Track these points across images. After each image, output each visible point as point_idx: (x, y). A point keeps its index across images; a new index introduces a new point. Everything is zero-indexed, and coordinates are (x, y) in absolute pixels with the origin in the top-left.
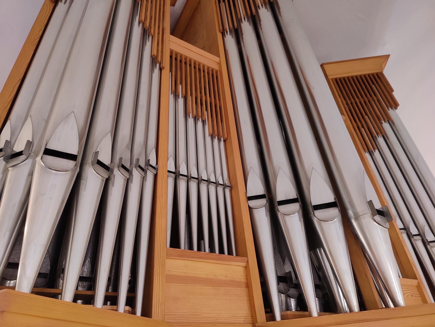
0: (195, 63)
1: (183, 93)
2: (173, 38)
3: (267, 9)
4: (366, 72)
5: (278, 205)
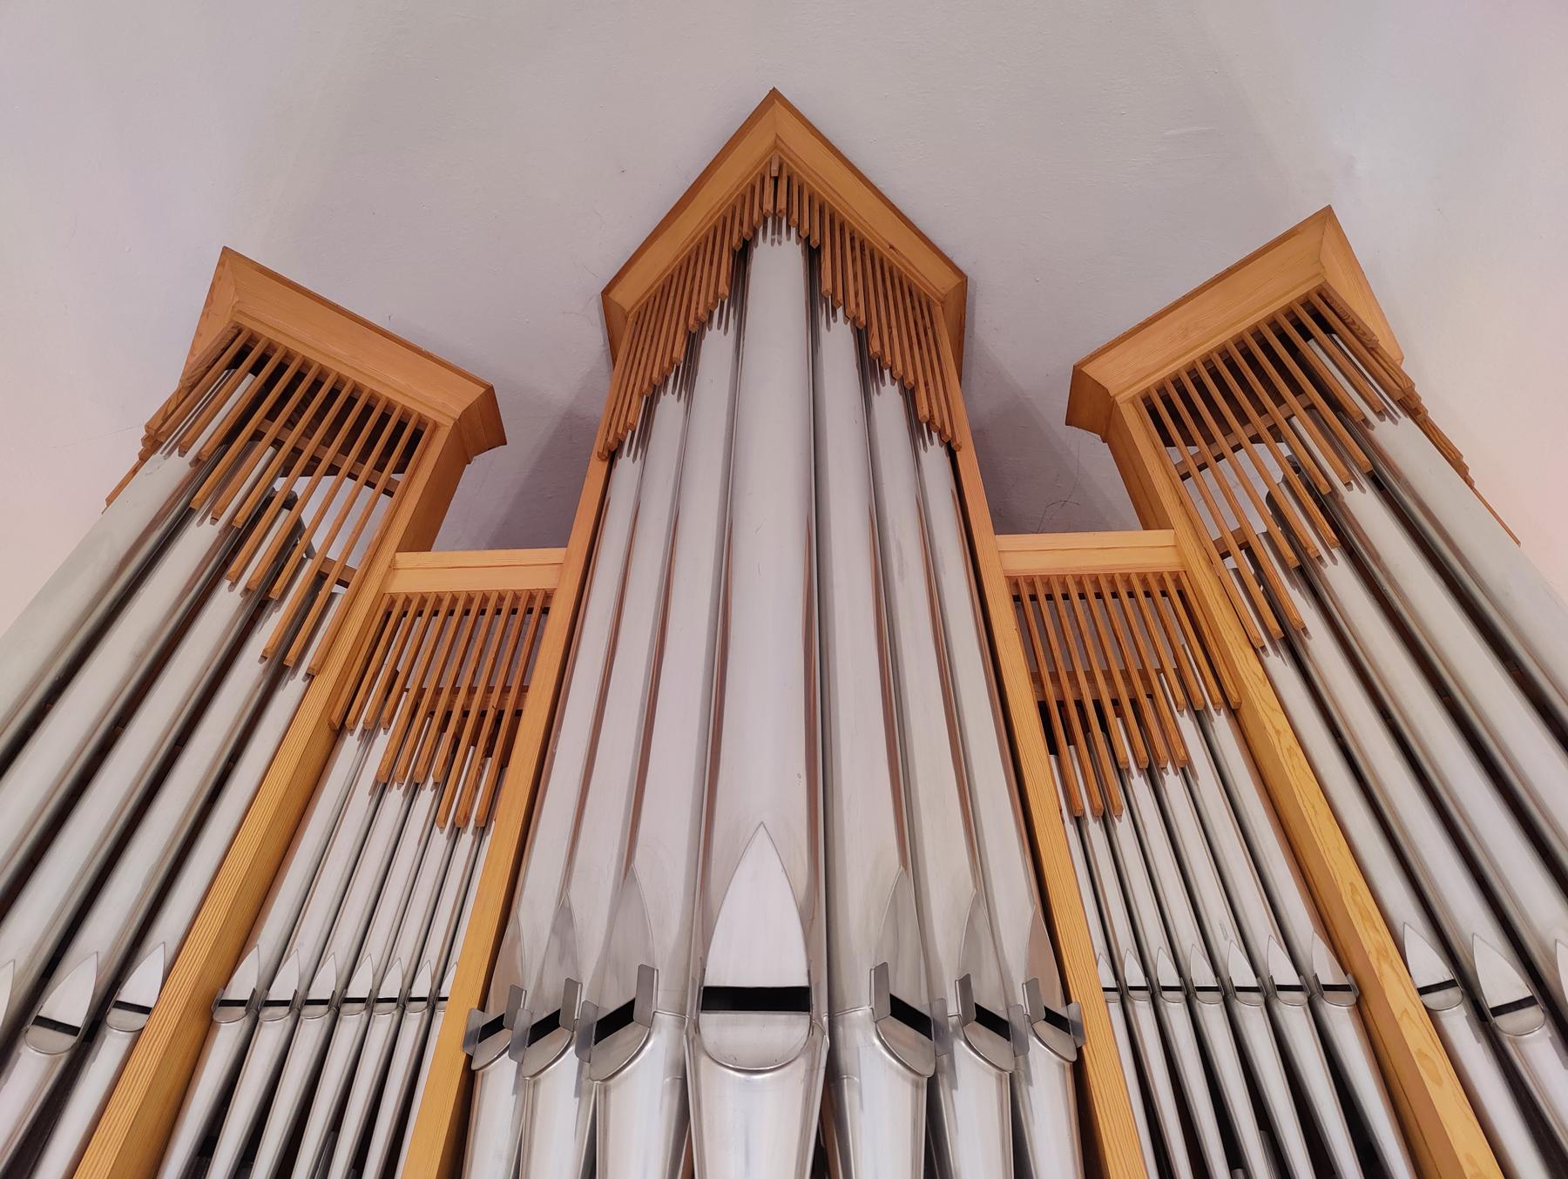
0: (1079, 582)
3: (578, 1099)
4: (1224, 337)
5: (1494, 1016)
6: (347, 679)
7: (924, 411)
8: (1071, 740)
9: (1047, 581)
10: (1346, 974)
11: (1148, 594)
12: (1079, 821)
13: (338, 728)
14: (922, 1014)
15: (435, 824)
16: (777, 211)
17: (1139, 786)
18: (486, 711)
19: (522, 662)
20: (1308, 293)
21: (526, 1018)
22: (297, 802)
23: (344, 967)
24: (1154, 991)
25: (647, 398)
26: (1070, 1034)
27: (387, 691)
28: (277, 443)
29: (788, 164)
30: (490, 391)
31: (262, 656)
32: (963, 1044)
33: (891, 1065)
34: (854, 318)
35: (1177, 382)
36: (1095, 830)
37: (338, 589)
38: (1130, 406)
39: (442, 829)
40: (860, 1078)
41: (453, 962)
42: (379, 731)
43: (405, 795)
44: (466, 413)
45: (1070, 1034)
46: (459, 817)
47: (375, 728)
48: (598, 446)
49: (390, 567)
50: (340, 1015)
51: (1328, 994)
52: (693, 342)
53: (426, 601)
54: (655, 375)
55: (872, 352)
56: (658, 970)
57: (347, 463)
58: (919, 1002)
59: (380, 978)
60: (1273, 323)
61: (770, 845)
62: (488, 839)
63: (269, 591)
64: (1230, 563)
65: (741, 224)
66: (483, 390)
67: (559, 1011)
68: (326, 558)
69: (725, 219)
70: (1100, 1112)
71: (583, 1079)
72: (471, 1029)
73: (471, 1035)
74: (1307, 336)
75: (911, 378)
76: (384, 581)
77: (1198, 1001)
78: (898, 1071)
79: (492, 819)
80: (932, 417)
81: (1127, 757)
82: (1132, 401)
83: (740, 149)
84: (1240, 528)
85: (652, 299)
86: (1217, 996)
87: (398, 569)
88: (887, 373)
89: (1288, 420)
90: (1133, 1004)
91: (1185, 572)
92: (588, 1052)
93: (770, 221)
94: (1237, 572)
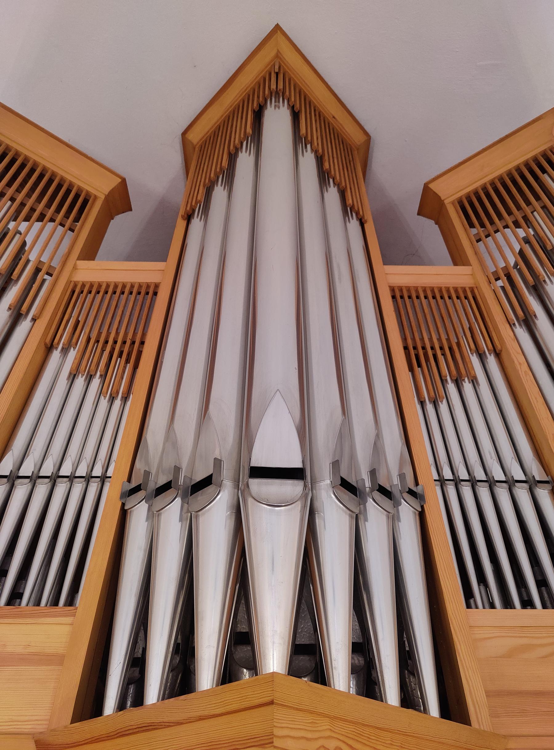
0: (425, 290)
1: (490, 349)
2: (390, 269)
3: (181, 523)
6: (62, 303)
7: (349, 201)
8: (419, 365)
9: (409, 289)
10: (548, 476)
11: (458, 298)
12: (422, 404)
13: (49, 346)
14: (355, 486)
15: (102, 395)
16: (278, 90)
17: (451, 388)
18: (126, 341)
19: (144, 317)
20: (545, 150)
21: (152, 486)
22: (30, 381)
23: (57, 461)
24: (457, 482)
25: (207, 187)
26: (417, 499)
27: (74, 330)
28: (13, 200)
29: (283, 66)
30: (124, 181)
31: (9, 308)
32: (371, 500)
33: (339, 506)
34: (316, 150)
35: (476, 193)
36: (430, 408)
37: (46, 277)
38: (451, 205)
39: (105, 397)
40: (324, 514)
41: (113, 460)
42: (70, 349)
43: (85, 380)
44: (110, 192)
45: (417, 499)
46: (114, 391)
47: (68, 347)
48: (182, 212)
49: (74, 267)
50: (56, 483)
51: (539, 485)
52: (233, 158)
53: (93, 286)
54: (212, 175)
55: (324, 169)
56: (223, 461)
57: (50, 213)
58: (352, 480)
59: (76, 468)
60: (527, 164)
61: (282, 400)
62: (129, 403)
63: (12, 274)
64: (500, 283)
65: (258, 97)
66: (120, 180)
67: (171, 481)
68: (40, 261)
69: (249, 96)
70: (432, 534)
71: (183, 513)
72: (124, 491)
73: (124, 493)
74: (544, 171)
75: (343, 184)
76: (71, 276)
77: (477, 486)
78: (343, 510)
79: (130, 394)
80: (353, 204)
81: (446, 374)
82: (453, 203)
83: (258, 57)
84: (506, 266)
85: (209, 138)
86: (486, 484)
87: (78, 269)
88: (331, 180)
89: (532, 213)
90: (446, 487)
91: (477, 287)
92: (187, 499)
93: (273, 94)
94: (503, 288)
